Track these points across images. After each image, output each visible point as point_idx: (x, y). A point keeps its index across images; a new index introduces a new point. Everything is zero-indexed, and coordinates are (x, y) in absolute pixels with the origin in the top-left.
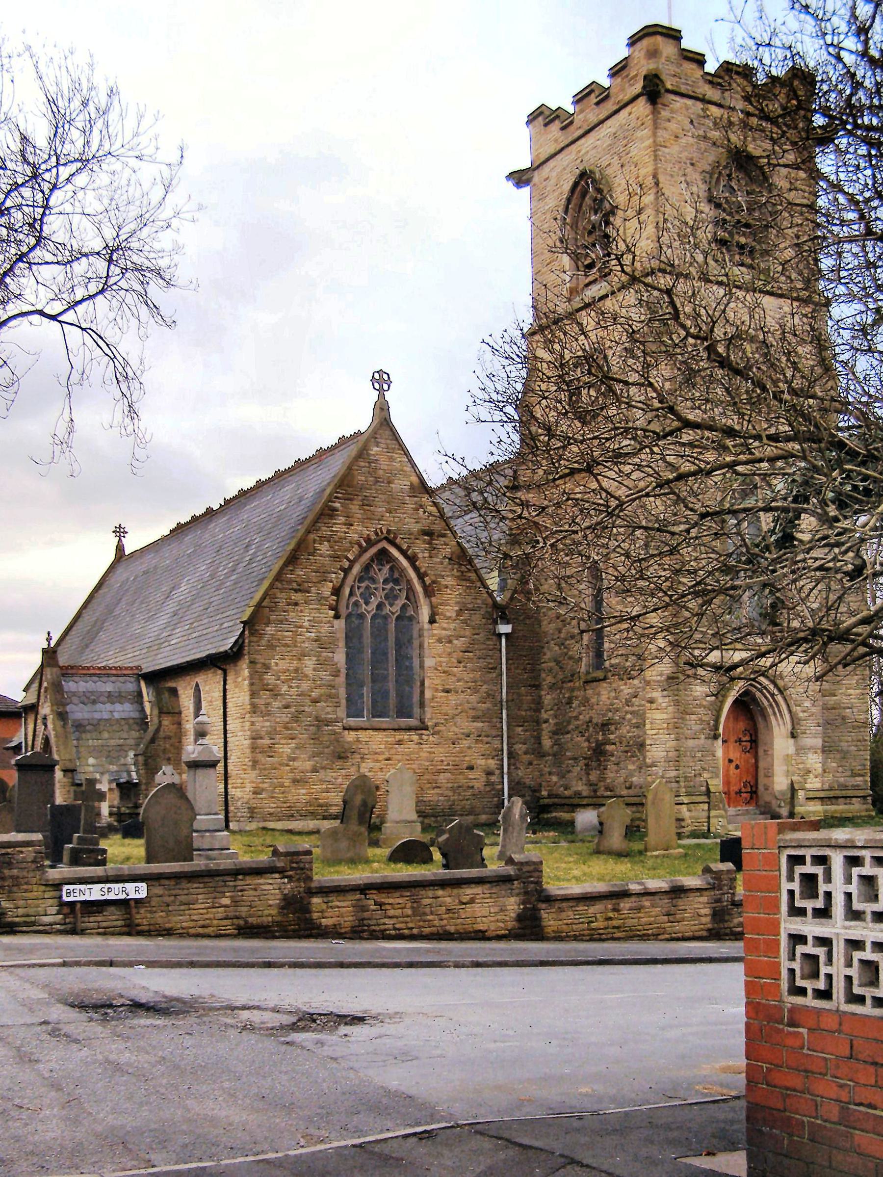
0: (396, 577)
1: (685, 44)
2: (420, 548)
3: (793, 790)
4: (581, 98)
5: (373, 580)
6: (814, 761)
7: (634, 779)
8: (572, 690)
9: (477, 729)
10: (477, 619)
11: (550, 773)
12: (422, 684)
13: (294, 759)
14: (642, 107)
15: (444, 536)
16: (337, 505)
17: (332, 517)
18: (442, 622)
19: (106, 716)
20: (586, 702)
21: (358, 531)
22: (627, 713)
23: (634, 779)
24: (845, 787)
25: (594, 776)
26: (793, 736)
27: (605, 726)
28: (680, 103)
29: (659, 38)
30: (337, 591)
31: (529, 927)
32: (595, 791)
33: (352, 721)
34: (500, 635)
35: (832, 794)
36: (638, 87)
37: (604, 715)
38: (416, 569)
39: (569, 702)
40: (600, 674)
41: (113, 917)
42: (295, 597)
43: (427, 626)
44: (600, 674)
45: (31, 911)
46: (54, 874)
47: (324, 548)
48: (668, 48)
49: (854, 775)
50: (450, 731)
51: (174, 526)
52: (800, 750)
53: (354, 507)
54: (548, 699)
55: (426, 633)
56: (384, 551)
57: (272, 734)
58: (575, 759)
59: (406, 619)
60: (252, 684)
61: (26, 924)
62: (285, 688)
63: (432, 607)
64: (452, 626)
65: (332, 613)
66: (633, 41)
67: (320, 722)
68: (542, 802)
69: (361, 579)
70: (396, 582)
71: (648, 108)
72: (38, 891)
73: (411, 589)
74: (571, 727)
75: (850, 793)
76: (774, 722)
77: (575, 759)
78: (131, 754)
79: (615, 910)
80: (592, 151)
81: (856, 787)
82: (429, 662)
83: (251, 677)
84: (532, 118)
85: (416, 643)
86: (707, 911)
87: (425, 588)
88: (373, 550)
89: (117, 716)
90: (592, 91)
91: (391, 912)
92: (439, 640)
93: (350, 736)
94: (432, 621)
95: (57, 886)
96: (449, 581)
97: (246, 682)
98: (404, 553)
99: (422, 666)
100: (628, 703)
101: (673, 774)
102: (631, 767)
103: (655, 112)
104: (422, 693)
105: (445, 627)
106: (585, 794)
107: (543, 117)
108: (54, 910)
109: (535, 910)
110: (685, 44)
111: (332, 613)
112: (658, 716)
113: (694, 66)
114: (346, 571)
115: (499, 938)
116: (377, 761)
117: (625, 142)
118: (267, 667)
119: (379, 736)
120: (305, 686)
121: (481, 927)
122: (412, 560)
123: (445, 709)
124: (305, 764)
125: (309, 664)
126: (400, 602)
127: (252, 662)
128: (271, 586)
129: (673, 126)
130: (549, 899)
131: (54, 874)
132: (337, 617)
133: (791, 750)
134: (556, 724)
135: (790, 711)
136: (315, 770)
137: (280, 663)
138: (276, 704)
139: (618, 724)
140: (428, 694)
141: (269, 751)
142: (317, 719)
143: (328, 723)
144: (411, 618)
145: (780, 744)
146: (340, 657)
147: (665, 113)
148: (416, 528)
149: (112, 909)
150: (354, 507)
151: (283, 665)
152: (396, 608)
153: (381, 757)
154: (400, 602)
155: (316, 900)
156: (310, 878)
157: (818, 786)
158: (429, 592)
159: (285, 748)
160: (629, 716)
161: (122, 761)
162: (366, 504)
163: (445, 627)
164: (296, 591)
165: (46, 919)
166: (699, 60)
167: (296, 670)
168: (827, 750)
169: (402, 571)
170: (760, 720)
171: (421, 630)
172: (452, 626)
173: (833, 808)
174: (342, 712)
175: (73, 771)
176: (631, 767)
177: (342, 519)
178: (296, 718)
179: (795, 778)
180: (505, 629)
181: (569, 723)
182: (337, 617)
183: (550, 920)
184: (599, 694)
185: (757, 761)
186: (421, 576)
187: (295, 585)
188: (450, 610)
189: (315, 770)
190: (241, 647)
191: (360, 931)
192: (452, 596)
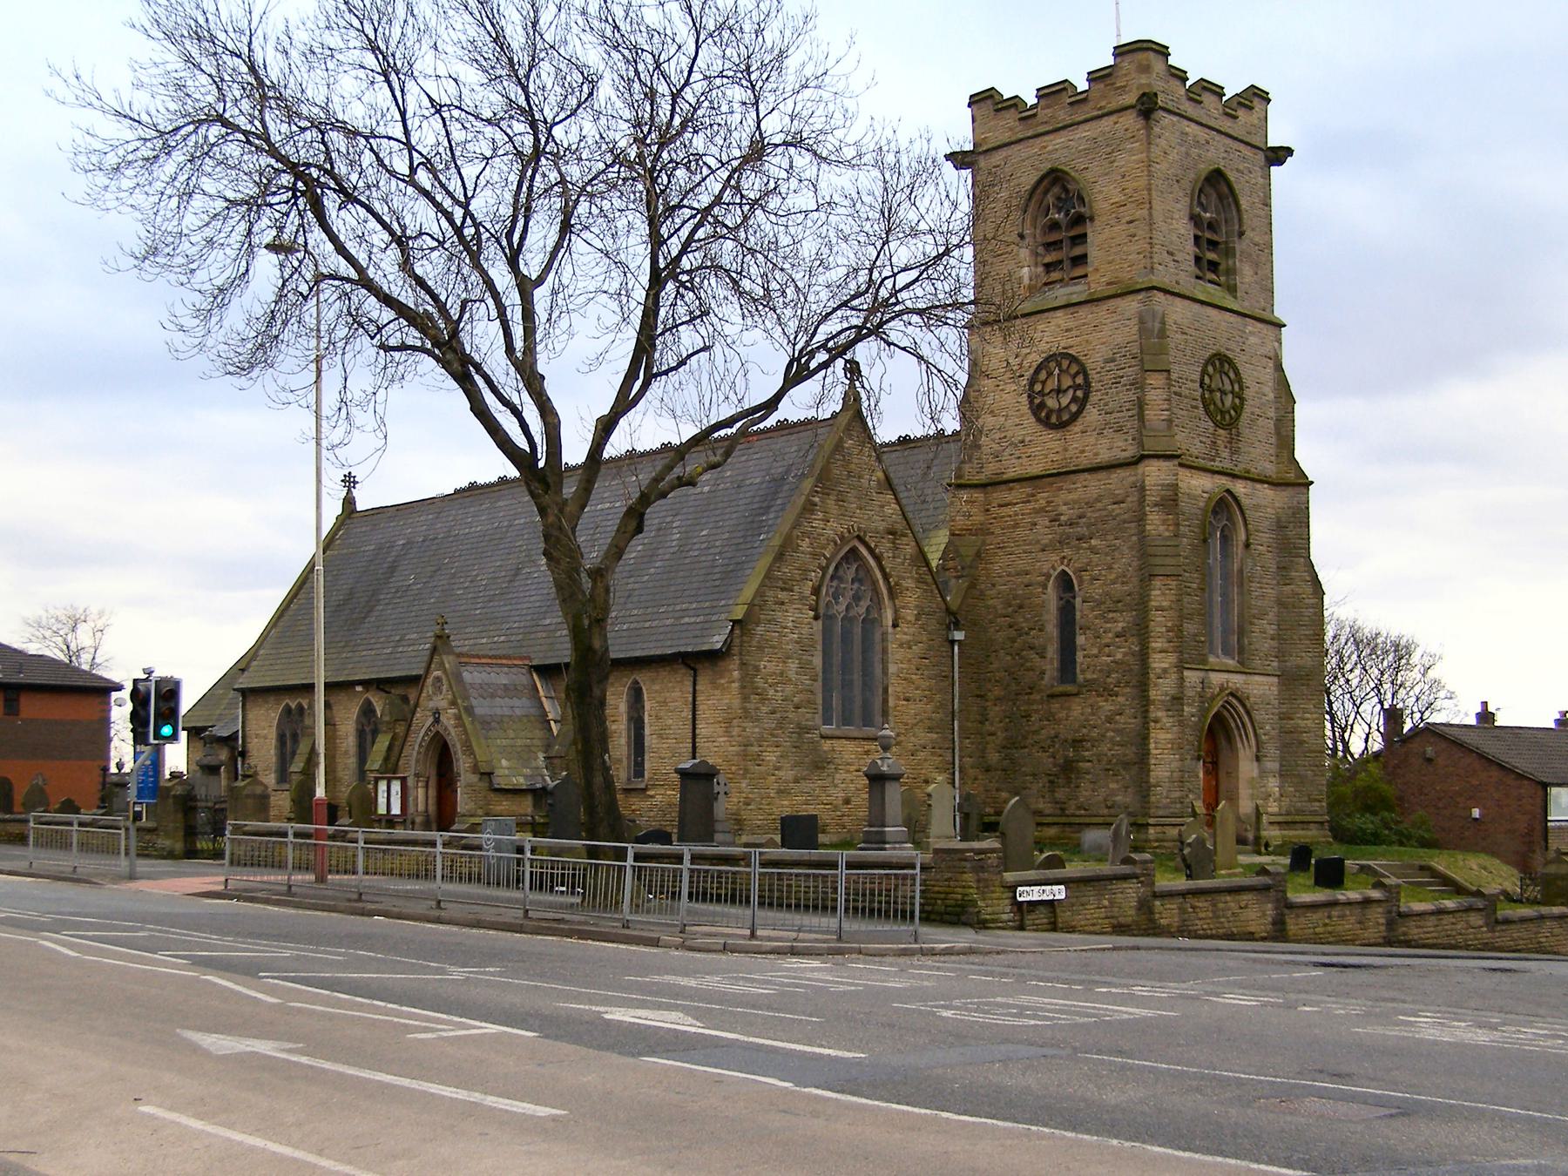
0: (863, 576)
1: (1171, 61)
2: (884, 548)
3: (1258, 814)
4: (1045, 93)
5: (841, 580)
6: (1273, 784)
7: (1118, 798)
8: (1030, 703)
9: (932, 741)
10: (933, 625)
11: (998, 790)
12: (886, 690)
13: (778, 769)
14: (1130, 120)
15: (905, 535)
16: (816, 499)
17: (812, 512)
18: (903, 626)
19: (507, 712)
20: (1050, 717)
21: (833, 529)
22: (1108, 730)
23: (1118, 798)
24: (1299, 812)
25: (1060, 794)
26: (1258, 759)
27: (1077, 743)
28: (1168, 119)
29: (1151, 55)
30: (816, 591)
31: (1279, 933)
32: (1063, 809)
33: (826, 729)
34: (952, 642)
35: (1289, 819)
36: (1131, 98)
37: (1077, 731)
38: (882, 569)
39: (1027, 716)
40: (1069, 688)
41: (1041, 916)
42: (782, 595)
43: (890, 630)
44: (1069, 688)
45: (996, 909)
46: (1010, 877)
47: (805, 544)
48: (1158, 66)
49: (1310, 800)
50: (911, 742)
51: (464, 484)
52: (1263, 773)
53: (831, 502)
54: (995, 711)
55: (890, 637)
56: (854, 550)
57: (760, 740)
58: (1034, 775)
59: (870, 623)
60: (743, 687)
61: (994, 921)
62: (771, 692)
63: (896, 611)
64: (912, 630)
65: (812, 613)
66: (1121, 51)
67: (803, 730)
68: (986, 820)
69: (832, 578)
70: (861, 581)
71: (1141, 122)
72: (998, 892)
73: (876, 590)
74: (1030, 741)
75: (1310, 818)
76: (1239, 745)
77: (1034, 775)
78: (541, 756)
79: (1329, 917)
80: (1060, 150)
81: (1314, 813)
82: (892, 669)
83: (742, 679)
84: (976, 100)
85: (878, 648)
86: (1382, 921)
87: (890, 589)
88: (847, 549)
89: (518, 712)
90: (1065, 89)
91: (1202, 915)
92: (901, 645)
93: (826, 745)
94: (895, 626)
95: (1012, 888)
96: (909, 583)
97: (736, 685)
98: (871, 551)
99: (885, 672)
100: (1110, 720)
101: (1178, 794)
102: (1113, 786)
103: (1149, 128)
104: (885, 701)
105: (906, 632)
106: (1047, 812)
107: (985, 102)
108: (1008, 909)
109: (1283, 915)
110: (1171, 61)
111: (812, 613)
112: (1162, 736)
113: (1178, 83)
114: (824, 569)
115: (1263, 939)
116: (848, 771)
117: (1109, 150)
118: (757, 669)
119: (850, 746)
120: (789, 689)
121: (1252, 929)
122: (878, 559)
123: (906, 718)
124: (787, 774)
125: (793, 665)
126: (865, 603)
127: (743, 664)
128: (762, 585)
129: (1162, 142)
130: (1291, 906)
131: (1010, 877)
132: (816, 618)
133: (1255, 773)
134: (1006, 738)
135: (1256, 735)
136: (796, 781)
137: (768, 665)
138: (764, 709)
139: (1095, 742)
140: (891, 703)
141: (758, 759)
142: (799, 726)
143: (808, 730)
144: (873, 621)
145: (1247, 767)
146: (817, 661)
147: (1157, 130)
148: (882, 526)
149: (1042, 908)
150: (831, 502)
151: (771, 667)
152: (862, 610)
153: (853, 768)
154: (865, 603)
155: (1158, 903)
156: (1153, 883)
157: (1276, 810)
158: (892, 594)
159: (771, 757)
160: (1110, 734)
161: (534, 764)
162: (840, 500)
163: (906, 632)
164: (783, 589)
165: (1005, 917)
166: (1181, 76)
167: (782, 674)
168: (1283, 775)
169: (868, 570)
170: (1223, 743)
171: (884, 634)
172: (912, 630)
173: (1292, 833)
174: (818, 720)
175: (490, 774)
176: (1113, 786)
177: (821, 515)
178: (780, 725)
179: (1260, 802)
180: (959, 635)
181: (1025, 738)
182: (816, 618)
183: (1292, 926)
184: (1069, 709)
185: (1217, 785)
186: (886, 577)
187: (780, 584)
188: (909, 614)
189: (796, 781)
190: (729, 648)
191: (1184, 931)
192: (912, 598)
